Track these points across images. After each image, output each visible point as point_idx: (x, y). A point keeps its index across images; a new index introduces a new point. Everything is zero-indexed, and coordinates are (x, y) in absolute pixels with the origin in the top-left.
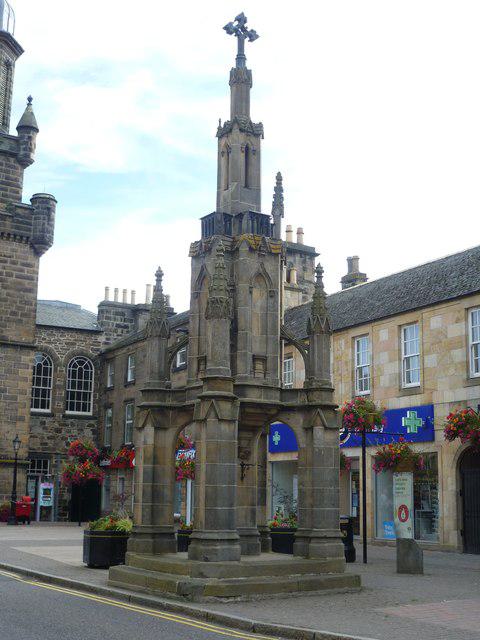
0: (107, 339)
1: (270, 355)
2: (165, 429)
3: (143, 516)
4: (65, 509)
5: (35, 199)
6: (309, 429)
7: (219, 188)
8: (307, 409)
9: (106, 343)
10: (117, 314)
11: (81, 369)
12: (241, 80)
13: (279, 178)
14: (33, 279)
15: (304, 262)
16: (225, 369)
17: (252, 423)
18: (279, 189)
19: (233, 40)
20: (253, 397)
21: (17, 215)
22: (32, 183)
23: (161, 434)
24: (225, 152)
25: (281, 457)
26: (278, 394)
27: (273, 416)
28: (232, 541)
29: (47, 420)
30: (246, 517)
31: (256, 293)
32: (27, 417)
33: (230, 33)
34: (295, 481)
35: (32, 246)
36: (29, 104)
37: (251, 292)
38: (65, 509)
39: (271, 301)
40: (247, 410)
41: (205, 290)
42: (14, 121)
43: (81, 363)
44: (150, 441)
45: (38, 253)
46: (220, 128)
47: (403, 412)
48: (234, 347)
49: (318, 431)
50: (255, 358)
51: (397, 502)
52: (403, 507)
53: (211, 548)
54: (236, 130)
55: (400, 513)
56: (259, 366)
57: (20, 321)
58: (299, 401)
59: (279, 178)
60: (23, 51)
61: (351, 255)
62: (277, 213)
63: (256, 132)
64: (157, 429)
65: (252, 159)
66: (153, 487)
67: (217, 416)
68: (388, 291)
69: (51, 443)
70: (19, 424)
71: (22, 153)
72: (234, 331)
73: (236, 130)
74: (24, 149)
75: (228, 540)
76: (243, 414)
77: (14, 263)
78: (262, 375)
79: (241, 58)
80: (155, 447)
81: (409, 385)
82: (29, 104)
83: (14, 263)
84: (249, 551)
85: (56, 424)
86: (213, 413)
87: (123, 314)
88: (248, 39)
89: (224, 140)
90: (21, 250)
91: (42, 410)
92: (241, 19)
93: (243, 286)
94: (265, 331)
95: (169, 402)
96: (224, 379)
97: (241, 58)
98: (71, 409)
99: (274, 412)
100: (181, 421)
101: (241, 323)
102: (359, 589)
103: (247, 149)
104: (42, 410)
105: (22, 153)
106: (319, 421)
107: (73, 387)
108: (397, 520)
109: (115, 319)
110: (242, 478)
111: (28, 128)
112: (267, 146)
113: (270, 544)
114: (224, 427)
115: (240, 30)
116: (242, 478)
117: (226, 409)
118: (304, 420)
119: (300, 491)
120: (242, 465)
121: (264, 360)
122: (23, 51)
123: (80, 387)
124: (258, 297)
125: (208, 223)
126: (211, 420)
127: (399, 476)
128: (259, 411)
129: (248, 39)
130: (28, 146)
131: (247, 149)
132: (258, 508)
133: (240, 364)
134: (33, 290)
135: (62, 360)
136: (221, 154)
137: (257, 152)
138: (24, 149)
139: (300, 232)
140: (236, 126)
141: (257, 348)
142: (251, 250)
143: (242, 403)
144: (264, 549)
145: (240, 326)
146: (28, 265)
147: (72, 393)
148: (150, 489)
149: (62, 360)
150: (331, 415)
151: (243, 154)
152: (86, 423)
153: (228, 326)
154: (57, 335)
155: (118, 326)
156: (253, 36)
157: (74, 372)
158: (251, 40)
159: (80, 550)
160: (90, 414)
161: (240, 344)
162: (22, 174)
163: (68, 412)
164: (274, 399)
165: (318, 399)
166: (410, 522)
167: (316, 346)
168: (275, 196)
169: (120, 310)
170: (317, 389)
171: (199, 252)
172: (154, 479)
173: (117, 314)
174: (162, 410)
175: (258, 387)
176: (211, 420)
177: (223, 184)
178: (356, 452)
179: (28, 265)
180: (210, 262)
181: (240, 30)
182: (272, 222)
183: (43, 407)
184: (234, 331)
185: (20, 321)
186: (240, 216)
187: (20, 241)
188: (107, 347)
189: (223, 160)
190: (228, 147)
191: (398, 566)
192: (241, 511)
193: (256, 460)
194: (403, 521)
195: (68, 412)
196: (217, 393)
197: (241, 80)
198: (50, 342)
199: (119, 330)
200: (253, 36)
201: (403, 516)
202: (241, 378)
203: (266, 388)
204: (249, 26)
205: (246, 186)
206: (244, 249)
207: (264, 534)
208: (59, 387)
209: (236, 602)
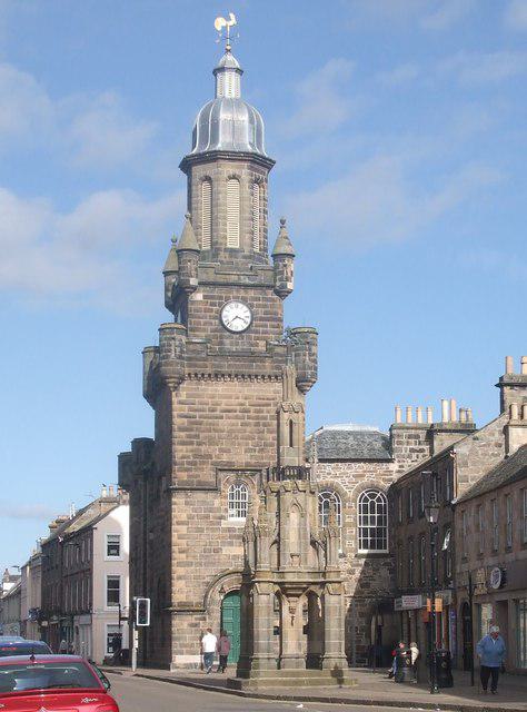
0: (400, 467)
4: (364, 655)
9: (399, 472)
10: (410, 437)
11: (373, 503)
21: (278, 354)
22: (128, 449)
38: (364, 655)
39: (317, 649)
43: (373, 496)
71: (278, 284)
74: (281, 280)
87: (417, 437)
103: (291, 422)
105: (278, 284)
107: (366, 523)
109: (408, 443)
123: (373, 523)
131: (291, 422)
135: (350, 494)
138: (281, 280)
149: (350, 494)
152: (382, 561)
155: (412, 450)
157: (365, 507)
160: (387, 551)
169: (413, 432)
173: (410, 437)
188: (401, 475)
198: (336, 477)
199: (414, 455)
208: (350, 525)
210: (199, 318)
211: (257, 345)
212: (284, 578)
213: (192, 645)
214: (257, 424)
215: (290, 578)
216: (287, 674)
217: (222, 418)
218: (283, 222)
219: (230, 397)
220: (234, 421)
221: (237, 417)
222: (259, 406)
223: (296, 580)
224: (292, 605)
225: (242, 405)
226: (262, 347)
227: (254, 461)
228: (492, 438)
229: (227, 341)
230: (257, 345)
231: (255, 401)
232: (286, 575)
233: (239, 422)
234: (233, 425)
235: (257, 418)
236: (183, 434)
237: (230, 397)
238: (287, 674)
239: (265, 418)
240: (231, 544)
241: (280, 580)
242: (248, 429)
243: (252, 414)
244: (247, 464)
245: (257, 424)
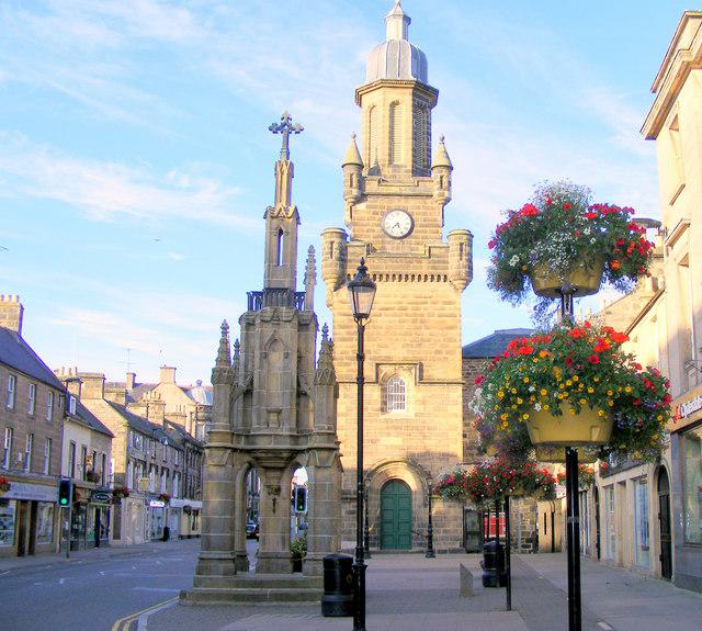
56: (273, 417)
116: (274, 511)
121: (279, 412)
122: (436, 92)
141: (277, 403)
146: (450, 303)
179: (450, 303)
181: (285, 128)
197: (286, 172)
210: (362, 225)
211: (417, 249)
212: (253, 443)
213: (350, 532)
214: (415, 321)
215: (262, 444)
216: (246, 584)
217: (380, 315)
218: (274, 511)
219: (388, 296)
220: (391, 318)
221: (396, 315)
222: (417, 303)
223: (271, 446)
224: (274, 483)
225: (400, 303)
226: (421, 250)
227: (411, 356)
228: (626, 312)
229: (388, 247)
230: (417, 249)
231: (412, 299)
232: (258, 440)
233: (397, 318)
234: (391, 322)
235: (415, 315)
236: (343, 331)
237: (388, 296)
238: (246, 584)
239: (422, 315)
240: (389, 435)
241: (248, 447)
242: (406, 325)
243: (410, 312)
244: (404, 358)
245: (415, 321)
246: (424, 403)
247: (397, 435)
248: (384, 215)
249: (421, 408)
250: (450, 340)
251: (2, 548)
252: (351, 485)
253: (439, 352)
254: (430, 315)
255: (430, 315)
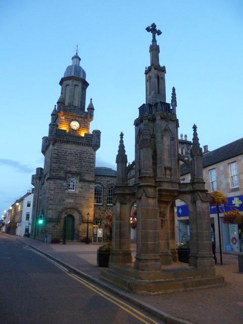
1: (173, 167)
2: (125, 204)
3: (116, 245)
5: (94, 132)
6: (194, 202)
7: (146, 95)
8: (193, 192)
12: (155, 50)
13: (174, 89)
14: (94, 159)
15: (188, 147)
16: (150, 172)
17: (165, 200)
18: (174, 95)
19: (150, 34)
20: (166, 186)
23: (124, 206)
24: (148, 80)
25: (182, 218)
26: (178, 186)
27: (176, 196)
28: (156, 260)
29: (101, 207)
30: (164, 246)
31: (165, 139)
32: (93, 206)
33: (149, 31)
34: (188, 227)
35: (93, 148)
36: (91, 101)
37: (162, 138)
38: (108, 238)
40: (163, 193)
41: (141, 138)
42: (87, 106)
44: (118, 210)
45: (95, 150)
46: (146, 70)
47: (232, 199)
48: (155, 164)
49: (199, 203)
50: (165, 169)
51: (232, 236)
52: (234, 238)
53: (145, 264)
54: (153, 69)
55: (233, 240)
56: (168, 172)
57: (89, 173)
58: (188, 188)
59: (174, 89)
60: (88, 84)
61: (205, 145)
62: (174, 104)
63: (163, 70)
64: (121, 204)
65: (161, 81)
66: (120, 231)
67: (146, 196)
68: (222, 152)
69: (102, 215)
70: (90, 208)
72: (155, 157)
73: (153, 69)
75: (155, 259)
76: (160, 195)
77: (87, 153)
78: (169, 177)
79: (154, 40)
80: (121, 213)
81: (234, 188)
82: (91, 101)
83: (87, 153)
84: (168, 263)
85: (104, 209)
86: (144, 194)
88: (157, 34)
89: (148, 75)
90: (90, 149)
91: (99, 204)
92: (154, 26)
93: (158, 135)
94: (170, 155)
95: (127, 192)
96: (150, 177)
97: (154, 40)
98: (109, 203)
99: (176, 194)
100: (133, 200)
101: (159, 152)
102: (224, 284)
103: (158, 77)
104: (99, 204)
106: (199, 198)
108: (232, 243)
110: (162, 227)
111: (91, 109)
112: (167, 77)
113: (178, 258)
114: (151, 201)
115: (153, 30)
116: (162, 227)
117: (151, 191)
118: (191, 198)
119: (191, 233)
120: (162, 220)
121: (170, 169)
122: (88, 84)
124: (167, 140)
125: (142, 109)
126: (144, 197)
127: (232, 225)
128: (169, 194)
129: (157, 34)
130: (91, 116)
132: (170, 241)
133: (158, 171)
134: (94, 162)
136: (147, 81)
137: (163, 79)
139: (186, 136)
140: (152, 67)
141: (167, 164)
142: (162, 118)
143: (160, 191)
144: (175, 260)
145: (157, 153)
146: (92, 154)
147: (109, 198)
148: (118, 232)
150: (204, 195)
151: (157, 79)
153: (150, 152)
154: (103, 178)
156: (159, 33)
158: (159, 34)
159: (95, 256)
161: (158, 162)
162: (89, 124)
163: (108, 204)
164: (176, 188)
165: (197, 187)
166: (237, 245)
167: (195, 161)
168: (172, 97)
170: (197, 183)
171: (137, 123)
172: (120, 229)
174: (124, 195)
175: (167, 182)
176: (144, 197)
177: (148, 93)
178: (214, 216)
179: (92, 154)
180: (142, 126)
181: (153, 30)
182: (171, 108)
183: (99, 203)
184: (155, 157)
185: (89, 173)
186: (156, 104)
187: (89, 146)
189: (148, 83)
190: (150, 78)
191: (240, 268)
192: (162, 243)
193: (168, 218)
194: (235, 244)
195: (108, 204)
196: (146, 184)
197: (155, 50)
200: (159, 33)
201: (234, 242)
202: (158, 178)
203: (171, 182)
204: (157, 28)
205: (159, 93)
206: (158, 118)
207: (173, 253)
209: (159, 294)
214: (80, 159)
236: (55, 160)
240: (69, 198)
246: (82, 188)
247: (72, 199)
248: (71, 122)
249: (81, 190)
250: (91, 167)
251: (4, 240)
252: (118, 214)
253: (87, 171)
254: (86, 158)
255: (86, 158)
